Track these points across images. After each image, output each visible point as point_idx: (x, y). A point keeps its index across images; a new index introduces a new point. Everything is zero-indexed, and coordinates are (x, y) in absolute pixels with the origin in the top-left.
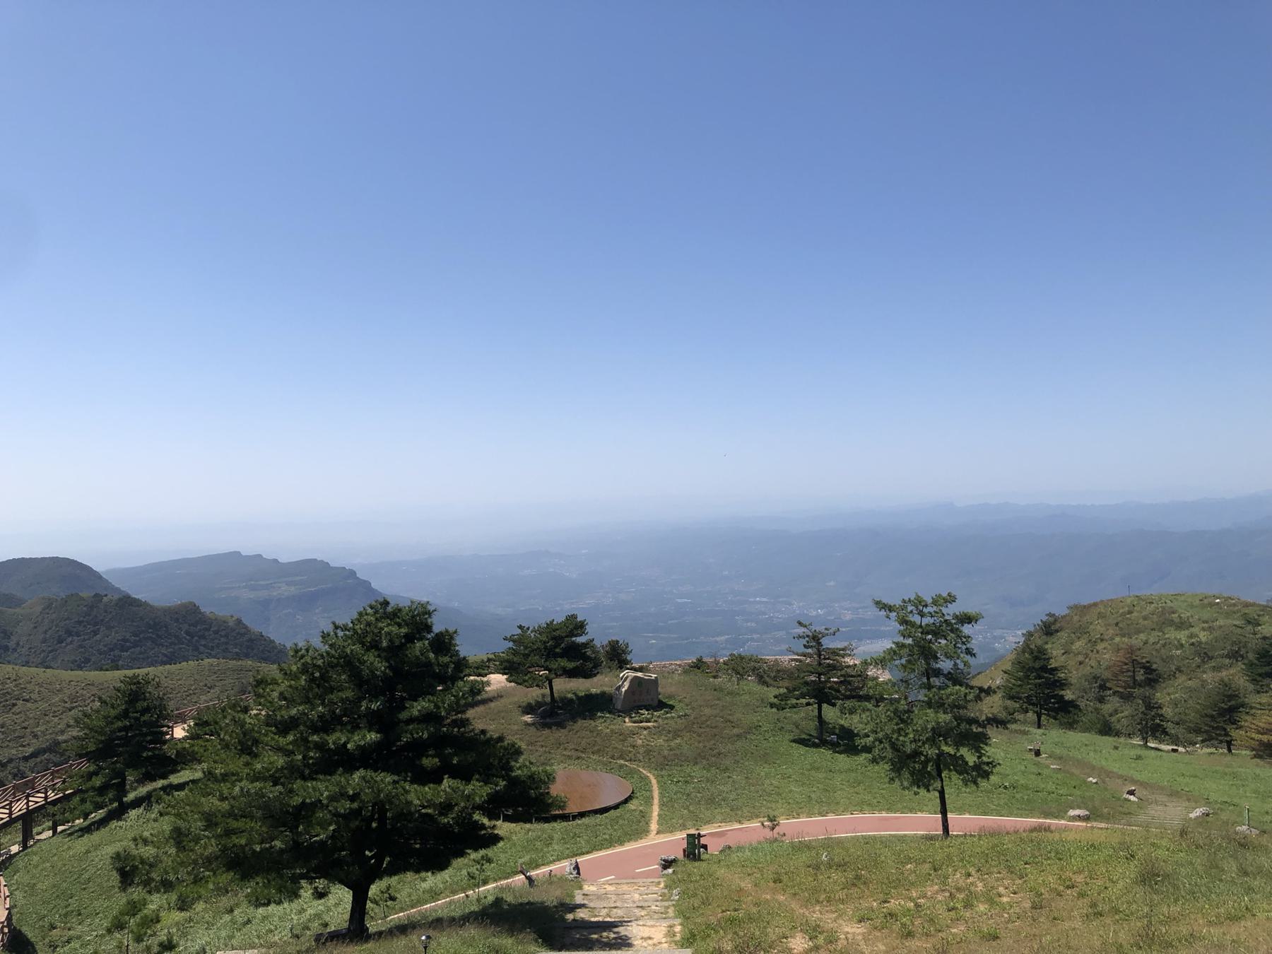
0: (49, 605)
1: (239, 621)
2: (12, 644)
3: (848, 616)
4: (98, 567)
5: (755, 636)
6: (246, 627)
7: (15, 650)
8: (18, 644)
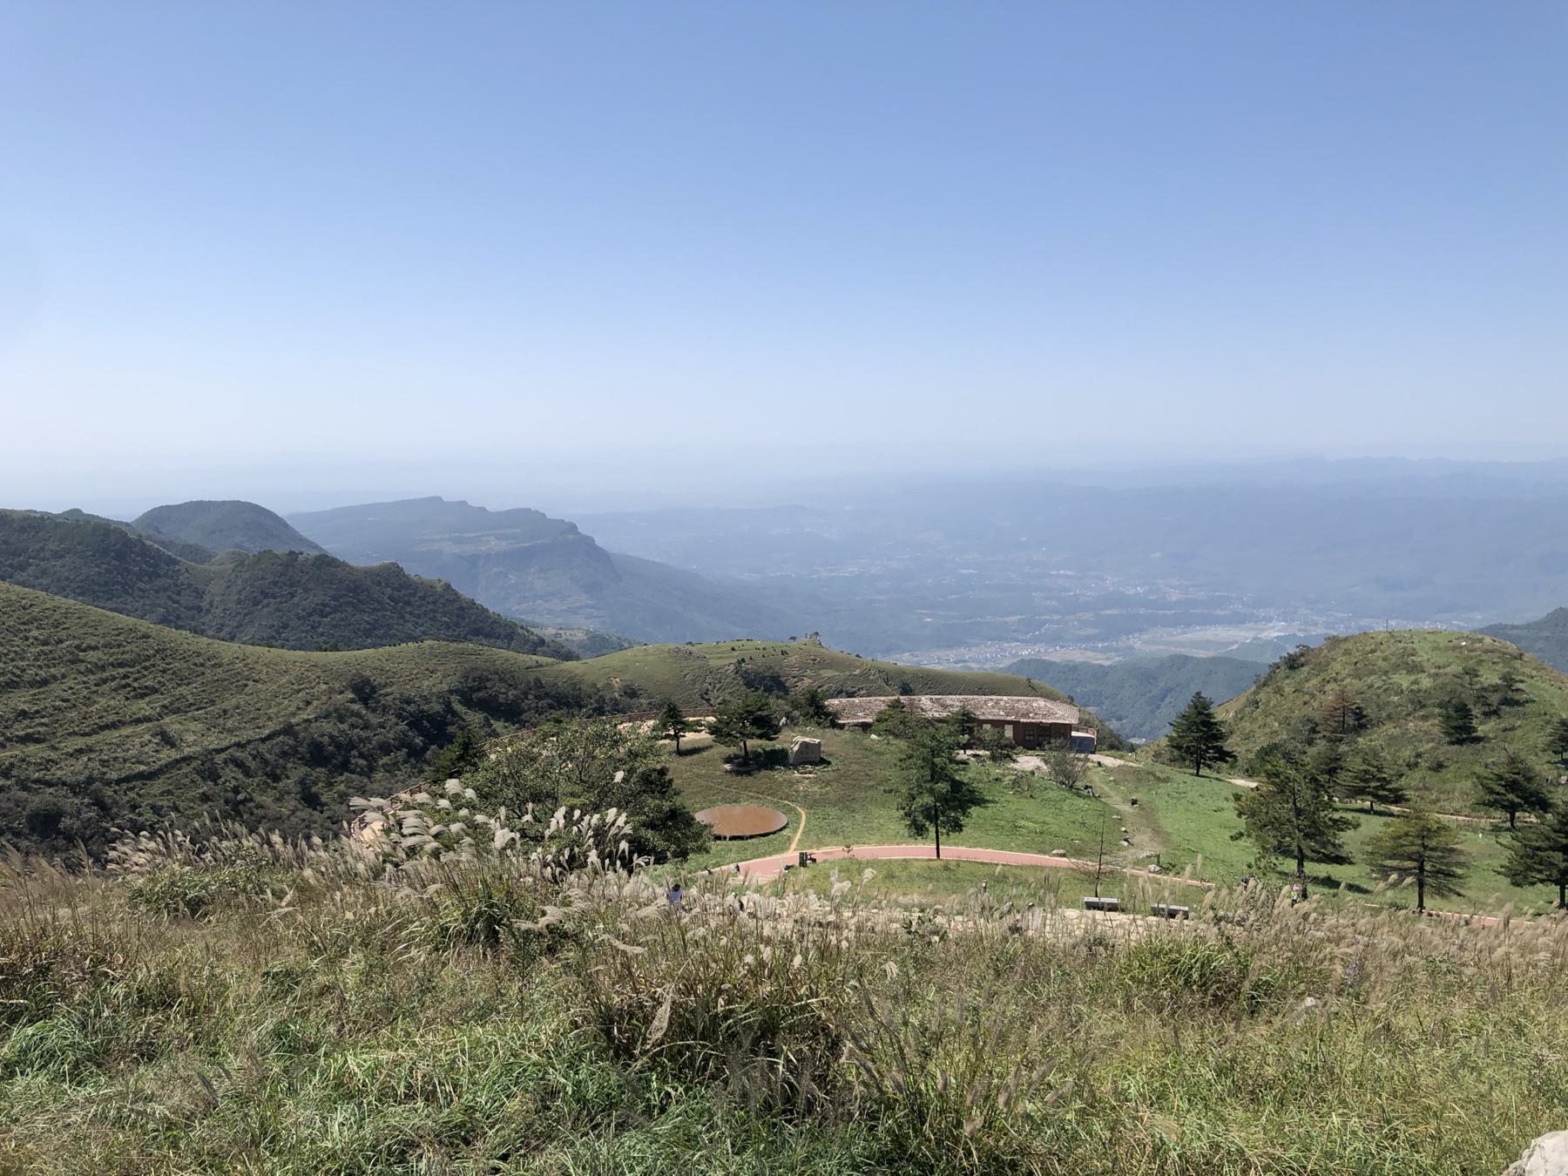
0: (240, 561)
1: (448, 587)
2: (205, 604)
3: (1175, 596)
4: (281, 510)
5: (1056, 617)
6: (456, 593)
7: (208, 611)
8: (211, 604)
